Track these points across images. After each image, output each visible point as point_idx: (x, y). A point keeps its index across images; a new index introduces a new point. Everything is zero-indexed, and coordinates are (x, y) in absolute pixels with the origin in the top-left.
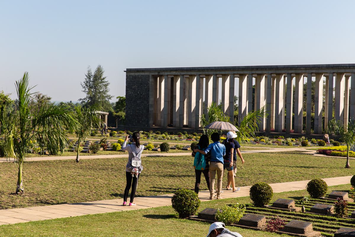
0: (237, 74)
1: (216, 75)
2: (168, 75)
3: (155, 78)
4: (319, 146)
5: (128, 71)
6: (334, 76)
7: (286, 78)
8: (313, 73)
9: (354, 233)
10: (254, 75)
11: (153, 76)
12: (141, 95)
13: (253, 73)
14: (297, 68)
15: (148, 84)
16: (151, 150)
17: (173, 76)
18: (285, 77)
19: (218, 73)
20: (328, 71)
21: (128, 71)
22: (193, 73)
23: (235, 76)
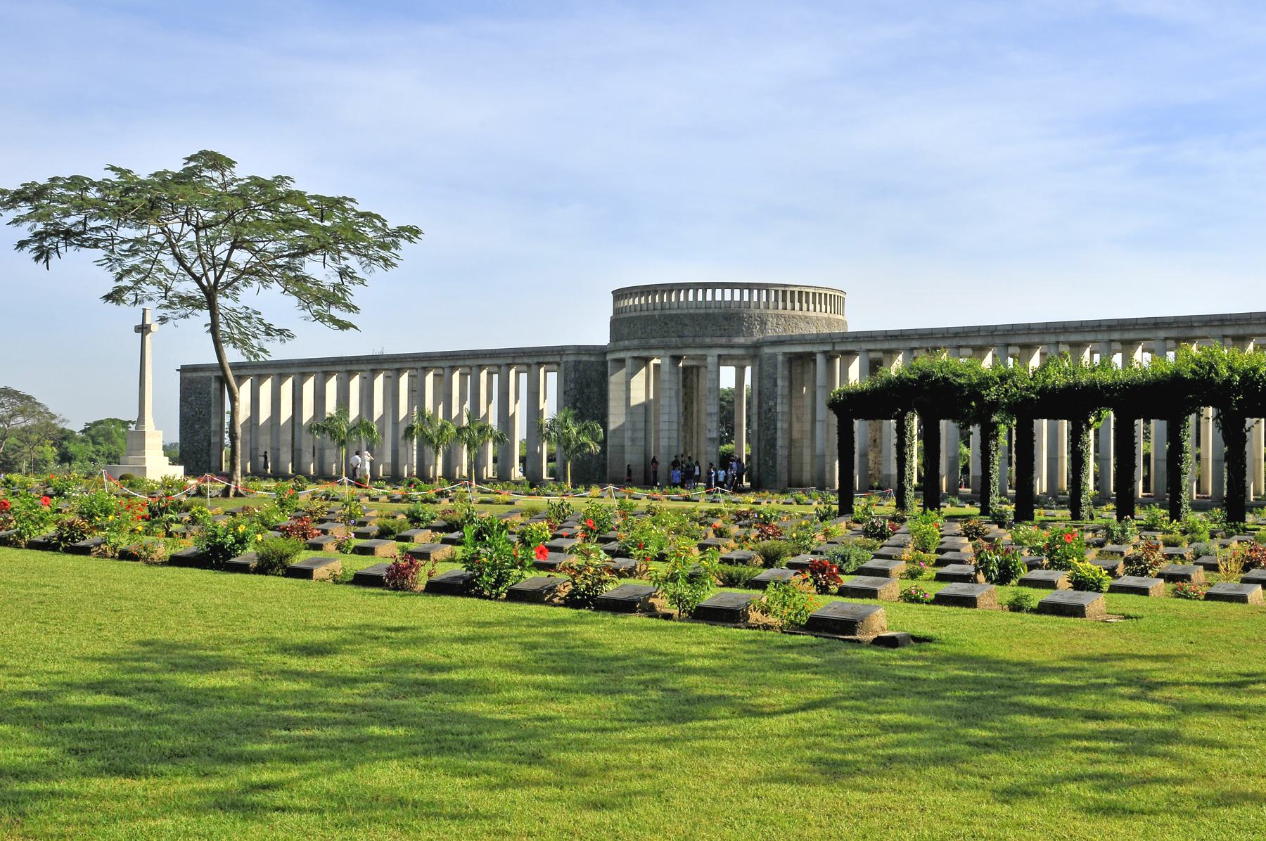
0: (967, 347)
1: (912, 350)
2: (1058, 343)
3: (830, 358)
4: (1010, 610)
5: (184, 370)
6: (1171, 350)
7: (496, 377)
8: (1114, 341)
9: (4, 737)
10: (1011, 350)
11: (825, 353)
12: (201, 413)
13: (1112, 338)
14: (1097, 326)
15: (209, 393)
16: (836, 589)
17: (880, 355)
18: (490, 374)
19: (915, 344)
20: (443, 364)
21: (184, 370)
22: (264, 372)
23: (1168, 347)
